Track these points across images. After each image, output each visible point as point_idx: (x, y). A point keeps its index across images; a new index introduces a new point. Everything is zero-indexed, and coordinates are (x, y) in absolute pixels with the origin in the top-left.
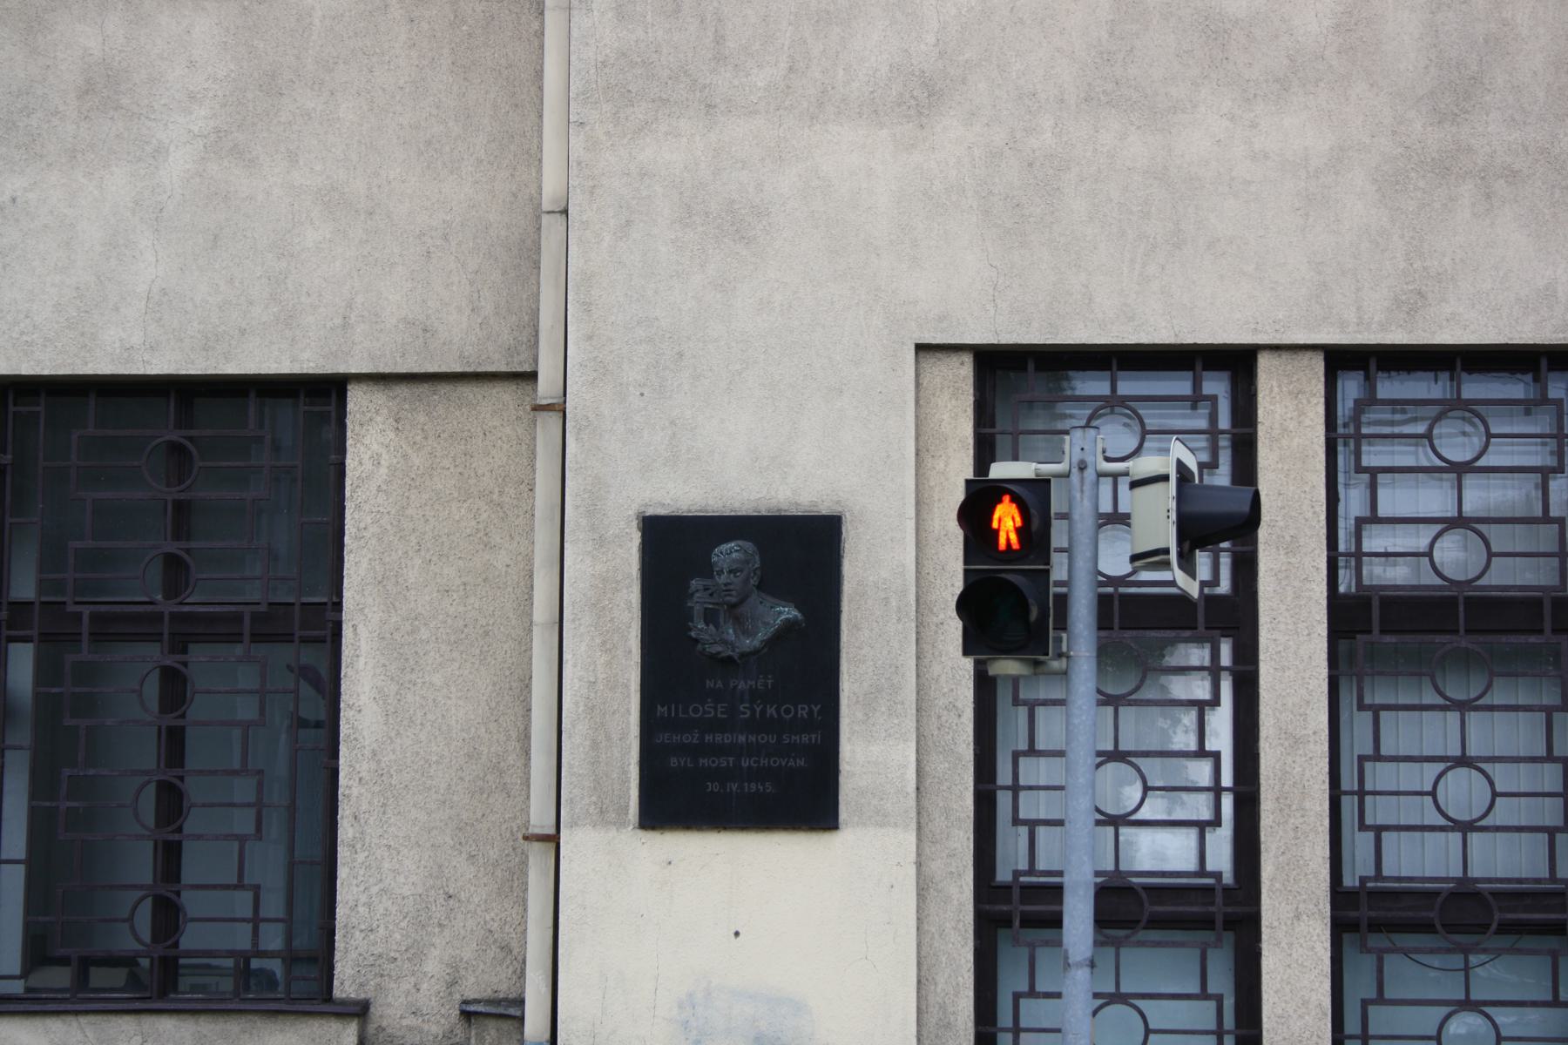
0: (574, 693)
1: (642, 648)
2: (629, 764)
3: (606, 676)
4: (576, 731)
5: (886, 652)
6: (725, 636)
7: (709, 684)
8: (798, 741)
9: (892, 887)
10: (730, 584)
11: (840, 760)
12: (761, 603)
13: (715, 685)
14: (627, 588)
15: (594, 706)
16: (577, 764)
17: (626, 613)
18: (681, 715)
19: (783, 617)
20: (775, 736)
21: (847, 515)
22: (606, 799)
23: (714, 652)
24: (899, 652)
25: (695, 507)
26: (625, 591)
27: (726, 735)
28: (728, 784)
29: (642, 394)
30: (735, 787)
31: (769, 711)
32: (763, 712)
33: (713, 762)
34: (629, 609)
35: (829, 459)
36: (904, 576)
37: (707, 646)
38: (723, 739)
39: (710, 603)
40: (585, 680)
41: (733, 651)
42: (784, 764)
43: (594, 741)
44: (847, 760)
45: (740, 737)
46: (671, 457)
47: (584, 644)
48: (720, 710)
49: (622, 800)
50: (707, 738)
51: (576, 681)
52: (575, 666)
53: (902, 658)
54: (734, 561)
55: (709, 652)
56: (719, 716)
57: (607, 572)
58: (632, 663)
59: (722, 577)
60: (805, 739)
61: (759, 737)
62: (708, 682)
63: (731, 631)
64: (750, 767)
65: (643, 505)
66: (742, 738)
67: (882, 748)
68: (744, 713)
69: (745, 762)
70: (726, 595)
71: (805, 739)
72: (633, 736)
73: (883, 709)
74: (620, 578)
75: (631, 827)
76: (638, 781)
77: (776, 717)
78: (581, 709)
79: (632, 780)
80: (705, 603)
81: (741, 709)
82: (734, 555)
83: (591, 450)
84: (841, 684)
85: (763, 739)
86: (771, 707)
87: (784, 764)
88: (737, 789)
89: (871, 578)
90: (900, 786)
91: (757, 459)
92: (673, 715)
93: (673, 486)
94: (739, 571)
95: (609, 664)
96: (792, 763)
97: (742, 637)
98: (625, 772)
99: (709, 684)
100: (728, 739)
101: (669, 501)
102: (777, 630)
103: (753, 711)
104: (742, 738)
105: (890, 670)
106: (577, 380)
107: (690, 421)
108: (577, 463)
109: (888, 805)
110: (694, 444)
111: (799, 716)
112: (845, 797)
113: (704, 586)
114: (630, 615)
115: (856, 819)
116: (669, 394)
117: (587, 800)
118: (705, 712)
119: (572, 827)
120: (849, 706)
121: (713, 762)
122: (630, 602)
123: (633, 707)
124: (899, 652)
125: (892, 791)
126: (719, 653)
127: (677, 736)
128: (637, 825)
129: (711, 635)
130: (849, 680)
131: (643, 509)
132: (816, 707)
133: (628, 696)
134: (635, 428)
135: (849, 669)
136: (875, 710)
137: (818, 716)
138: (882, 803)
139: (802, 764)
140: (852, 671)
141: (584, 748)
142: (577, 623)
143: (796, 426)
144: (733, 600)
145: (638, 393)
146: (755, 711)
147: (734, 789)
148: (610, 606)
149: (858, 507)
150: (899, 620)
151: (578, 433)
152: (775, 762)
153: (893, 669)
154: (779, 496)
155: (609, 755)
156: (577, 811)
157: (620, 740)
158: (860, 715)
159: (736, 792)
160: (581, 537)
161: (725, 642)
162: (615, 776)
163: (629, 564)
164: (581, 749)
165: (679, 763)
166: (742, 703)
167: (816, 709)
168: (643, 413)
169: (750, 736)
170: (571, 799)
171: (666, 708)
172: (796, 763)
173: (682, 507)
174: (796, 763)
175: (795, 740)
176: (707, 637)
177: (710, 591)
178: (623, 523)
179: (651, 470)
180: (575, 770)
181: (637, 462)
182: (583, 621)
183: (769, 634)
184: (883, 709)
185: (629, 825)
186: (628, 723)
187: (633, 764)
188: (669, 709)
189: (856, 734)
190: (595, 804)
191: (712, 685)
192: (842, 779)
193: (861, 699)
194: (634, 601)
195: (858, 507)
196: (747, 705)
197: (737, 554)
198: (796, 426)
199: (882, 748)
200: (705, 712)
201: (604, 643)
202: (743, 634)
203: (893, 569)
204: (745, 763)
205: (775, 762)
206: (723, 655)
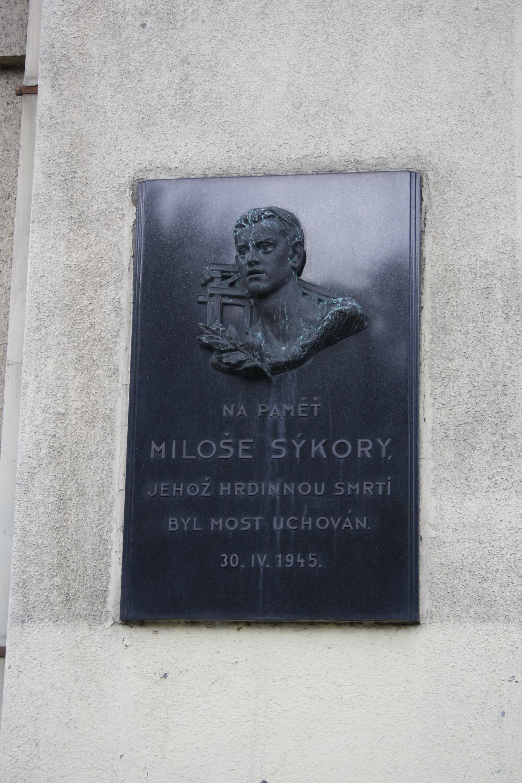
0: (35, 429)
1: (133, 372)
2: (110, 530)
3: (80, 404)
4: (36, 484)
5: (490, 365)
6: (250, 339)
7: (227, 410)
8: (357, 492)
9: (503, 714)
10: (257, 263)
11: (421, 522)
12: (304, 294)
13: (236, 410)
14: (115, 283)
15: (62, 448)
16: (35, 529)
17: (112, 316)
18: (184, 457)
19: (335, 309)
20: (323, 485)
21: (430, 174)
22: (75, 580)
23: (233, 362)
24: (508, 364)
25: (213, 171)
26: (112, 287)
27: (250, 484)
28: (253, 556)
29: (144, 25)
30: (262, 560)
31: (314, 449)
32: (306, 450)
33: (231, 523)
34: (117, 311)
35: (404, 101)
36: (514, 256)
37: (224, 355)
38: (245, 491)
39: (230, 296)
40: (52, 410)
41: (262, 360)
42: (335, 526)
43: (61, 498)
44: (431, 521)
45: (271, 486)
46: (181, 106)
47: (51, 361)
48: (241, 447)
49: (98, 583)
50: (222, 488)
51: (38, 412)
52: (38, 391)
53: (512, 373)
54: (263, 230)
55: (228, 364)
56: (241, 456)
57: (88, 261)
58: (119, 386)
59: (246, 256)
60: (368, 489)
61: (300, 487)
62: (225, 408)
63: (260, 334)
64: (285, 531)
65: (140, 171)
66: (274, 489)
67: (484, 503)
68: (278, 452)
69: (278, 523)
70: (251, 280)
71: (368, 489)
72: (116, 490)
73: (485, 447)
74: (105, 269)
75: (111, 622)
76: (121, 555)
77: (325, 456)
78: (44, 451)
79: (113, 553)
80: (224, 296)
81: (273, 445)
82: (264, 223)
83: (70, 100)
84: (421, 411)
85: (305, 488)
86: (316, 444)
87: (335, 526)
88: (266, 563)
89: (465, 261)
90: (512, 559)
91: (301, 104)
92: (174, 456)
93: (183, 143)
94: (271, 244)
95: (85, 388)
96: (348, 524)
97: (275, 342)
98: (104, 542)
99: (227, 410)
100: (253, 490)
101: (176, 164)
102: (326, 329)
103: (291, 449)
104: (274, 489)
105: (495, 390)
106: (56, 9)
107: (208, 58)
108: (52, 117)
109: (496, 588)
110: (213, 88)
111: (359, 455)
112: (430, 577)
113: (223, 272)
114: (118, 320)
115: (446, 609)
116: (179, 24)
117: (46, 583)
118: (220, 451)
119: (23, 622)
120: (433, 442)
121: (231, 523)
122: (119, 301)
123: (118, 449)
124: (508, 364)
125: (500, 567)
126: (240, 363)
127: (178, 486)
128: (118, 619)
129: (230, 339)
130: (433, 405)
131: (140, 175)
132: (384, 441)
133: (112, 433)
134: (132, 69)
135: (433, 389)
136: (473, 447)
137: (388, 453)
138: (485, 585)
139: (364, 526)
140: (438, 392)
141: (46, 507)
142: (43, 332)
143: (356, 58)
144: (263, 285)
145: (138, 24)
146: (294, 448)
147: (261, 564)
148: (90, 307)
149: (445, 164)
150: (507, 319)
151: (55, 78)
152: (322, 522)
153: (499, 388)
154: (332, 153)
155: (81, 517)
156: (31, 598)
157: (98, 495)
158: (450, 456)
159: (265, 569)
160: (53, 216)
161: (250, 348)
162: (88, 547)
163: (118, 250)
164: (42, 509)
165: (181, 524)
166: (275, 436)
167: (384, 445)
168: (144, 49)
169: (286, 486)
170: (24, 581)
171: (163, 446)
172: (354, 525)
173: (195, 172)
174: (354, 525)
175: (354, 491)
176: (225, 341)
177: (230, 281)
178: (113, 195)
179: (153, 124)
180: (32, 538)
181: (134, 113)
182: (51, 329)
183: (315, 336)
184: (485, 447)
185: (106, 620)
186: (110, 471)
187: (115, 531)
188: (168, 449)
189: (444, 485)
190: (59, 587)
191: (231, 413)
192: (424, 550)
193: (451, 432)
194: (123, 300)
195: (445, 164)
196: (282, 440)
197: (268, 221)
198: (356, 58)
199: (484, 503)
200: (220, 451)
201: (80, 358)
202: (278, 337)
203: (497, 247)
204: (278, 525)
205: (322, 522)
206: (247, 365)
